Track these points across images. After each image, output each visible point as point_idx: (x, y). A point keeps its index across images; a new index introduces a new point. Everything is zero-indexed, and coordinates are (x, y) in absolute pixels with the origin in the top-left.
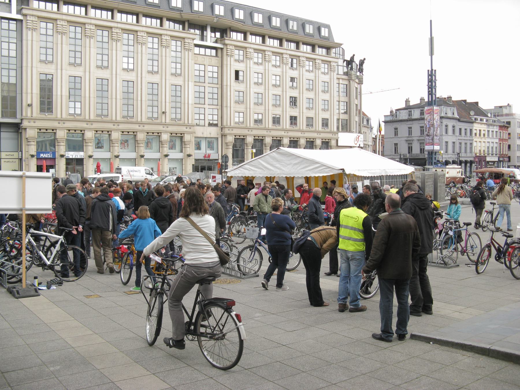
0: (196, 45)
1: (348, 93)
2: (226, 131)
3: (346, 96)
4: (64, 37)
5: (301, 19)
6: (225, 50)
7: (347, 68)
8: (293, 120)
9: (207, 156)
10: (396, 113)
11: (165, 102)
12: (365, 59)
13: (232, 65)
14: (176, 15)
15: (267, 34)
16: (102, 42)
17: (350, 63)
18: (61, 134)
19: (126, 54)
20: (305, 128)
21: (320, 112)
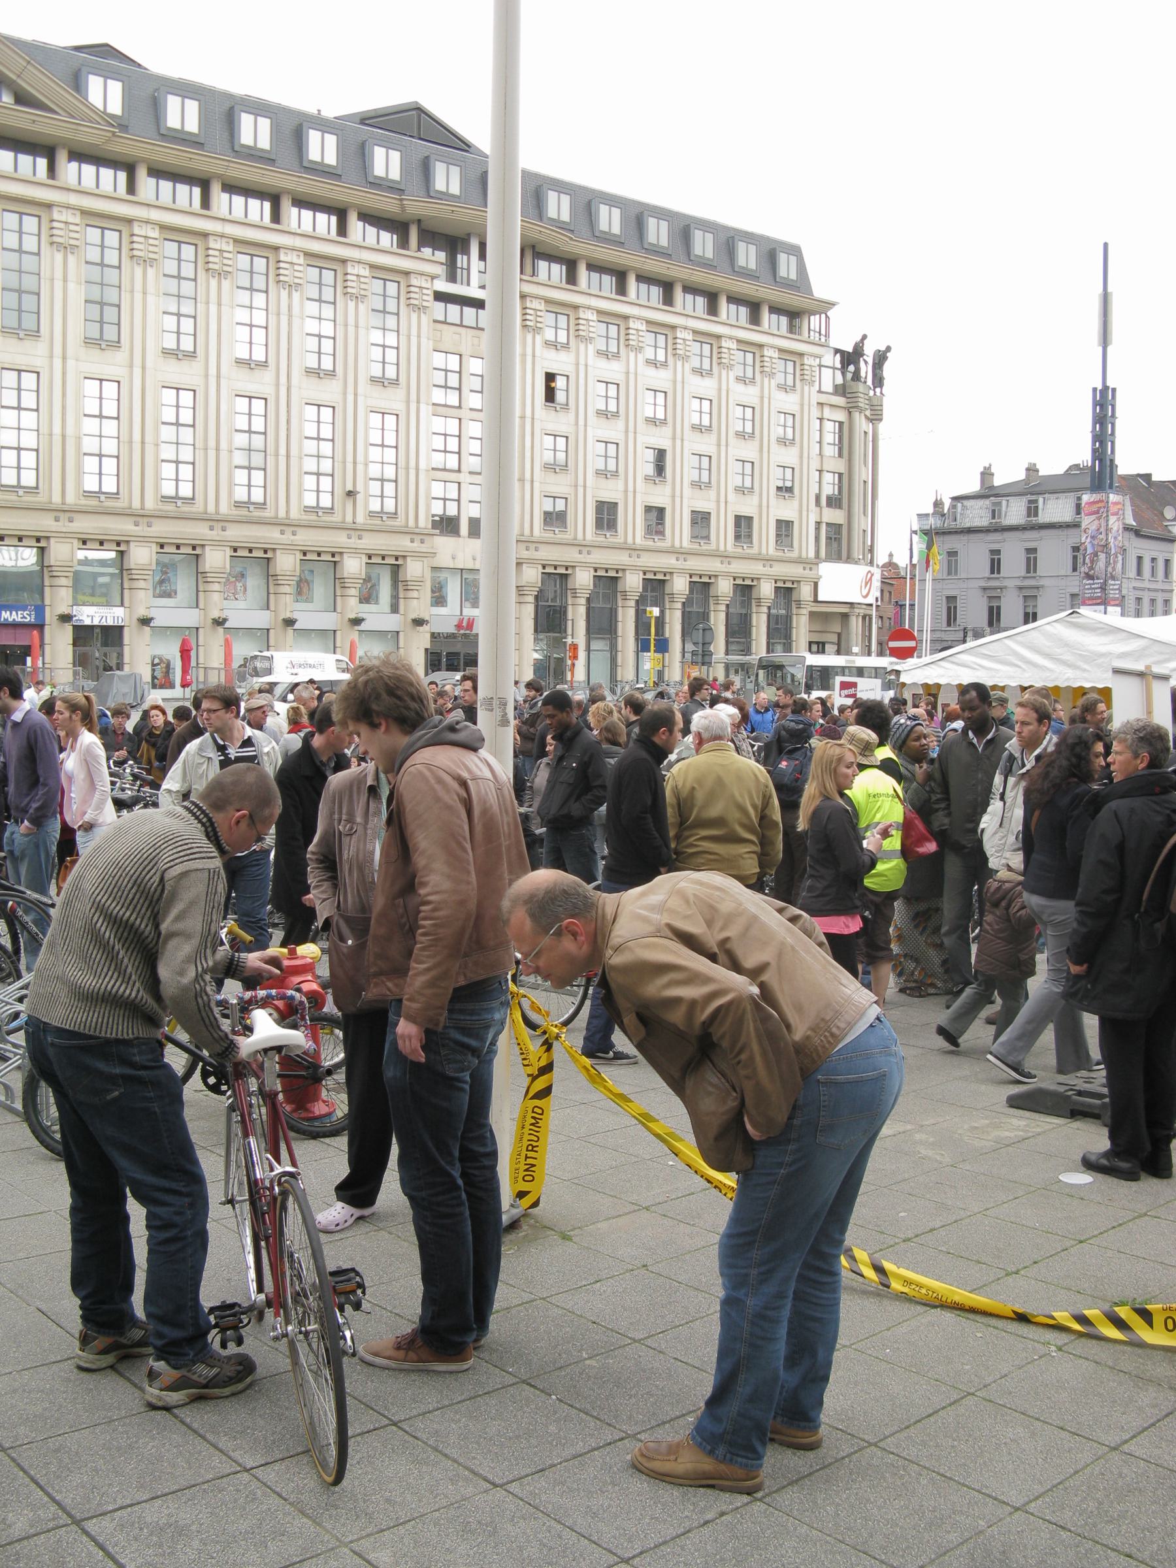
0: (440, 297)
1: (845, 445)
3: (840, 455)
4: (151, 272)
7: (843, 374)
8: (657, 516)
9: (465, 624)
10: (954, 507)
12: (888, 349)
14: (387, 204)
15: (288, 192)
17: (850, 358)
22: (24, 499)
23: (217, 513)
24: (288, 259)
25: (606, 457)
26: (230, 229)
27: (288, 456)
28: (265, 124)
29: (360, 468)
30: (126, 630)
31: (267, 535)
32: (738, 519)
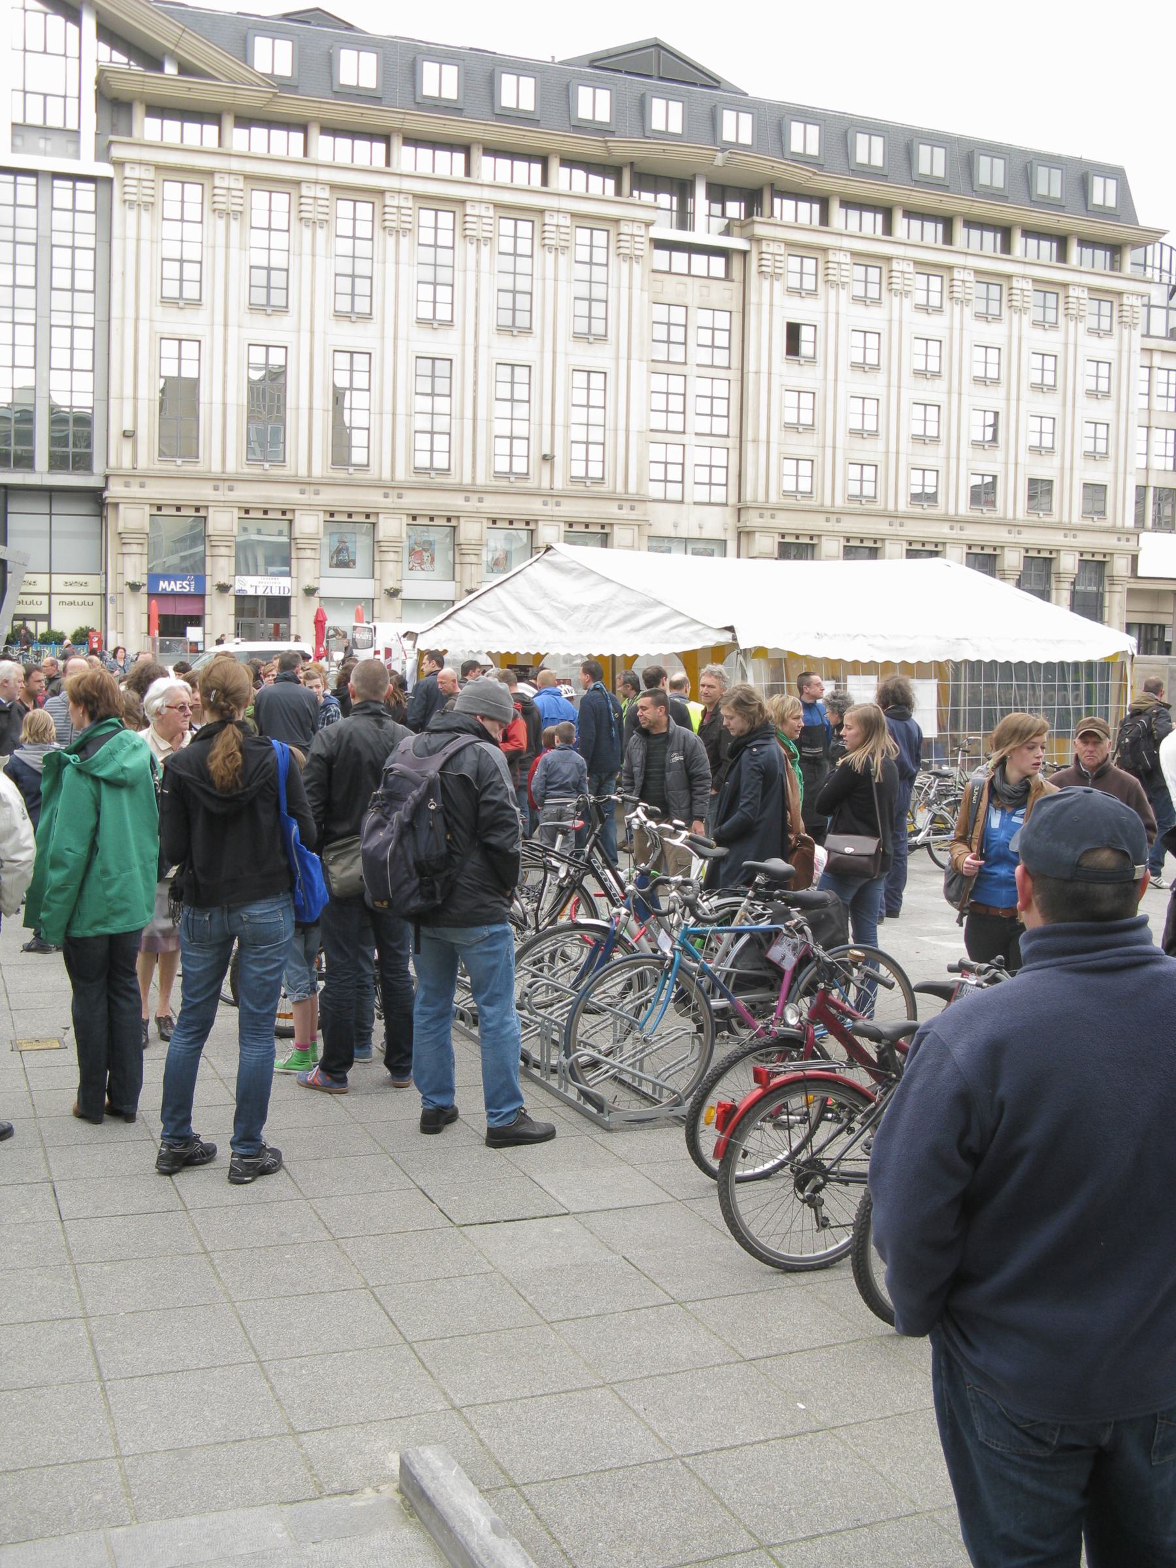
2: (752, 519)
5: (1024, 153)
6: (754, 257)
11: (553, 424)
13: (774, 307)
14: (591, 147)
16: (591, 263)
18: (221, 522)
19: (427, 273)
20: (1076, 519)
21: (1079, 461)
22: (184, 468)
23: (896, 510)
24: (476, 212)
25: (1095, 438)
26: (407, 185)
27: (475, 419)
28: (813, 131)
29: (559, 430)
30: (293, 600)
31: (449, 502)
32: (1033, 482)
